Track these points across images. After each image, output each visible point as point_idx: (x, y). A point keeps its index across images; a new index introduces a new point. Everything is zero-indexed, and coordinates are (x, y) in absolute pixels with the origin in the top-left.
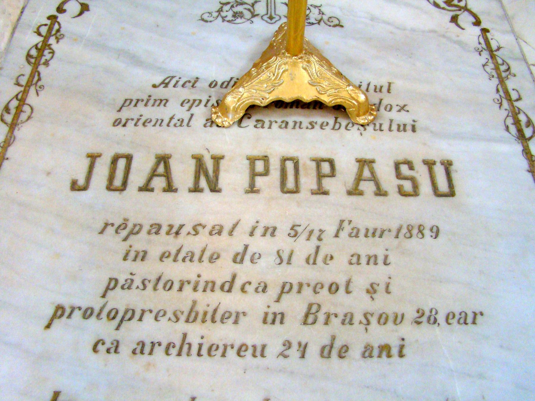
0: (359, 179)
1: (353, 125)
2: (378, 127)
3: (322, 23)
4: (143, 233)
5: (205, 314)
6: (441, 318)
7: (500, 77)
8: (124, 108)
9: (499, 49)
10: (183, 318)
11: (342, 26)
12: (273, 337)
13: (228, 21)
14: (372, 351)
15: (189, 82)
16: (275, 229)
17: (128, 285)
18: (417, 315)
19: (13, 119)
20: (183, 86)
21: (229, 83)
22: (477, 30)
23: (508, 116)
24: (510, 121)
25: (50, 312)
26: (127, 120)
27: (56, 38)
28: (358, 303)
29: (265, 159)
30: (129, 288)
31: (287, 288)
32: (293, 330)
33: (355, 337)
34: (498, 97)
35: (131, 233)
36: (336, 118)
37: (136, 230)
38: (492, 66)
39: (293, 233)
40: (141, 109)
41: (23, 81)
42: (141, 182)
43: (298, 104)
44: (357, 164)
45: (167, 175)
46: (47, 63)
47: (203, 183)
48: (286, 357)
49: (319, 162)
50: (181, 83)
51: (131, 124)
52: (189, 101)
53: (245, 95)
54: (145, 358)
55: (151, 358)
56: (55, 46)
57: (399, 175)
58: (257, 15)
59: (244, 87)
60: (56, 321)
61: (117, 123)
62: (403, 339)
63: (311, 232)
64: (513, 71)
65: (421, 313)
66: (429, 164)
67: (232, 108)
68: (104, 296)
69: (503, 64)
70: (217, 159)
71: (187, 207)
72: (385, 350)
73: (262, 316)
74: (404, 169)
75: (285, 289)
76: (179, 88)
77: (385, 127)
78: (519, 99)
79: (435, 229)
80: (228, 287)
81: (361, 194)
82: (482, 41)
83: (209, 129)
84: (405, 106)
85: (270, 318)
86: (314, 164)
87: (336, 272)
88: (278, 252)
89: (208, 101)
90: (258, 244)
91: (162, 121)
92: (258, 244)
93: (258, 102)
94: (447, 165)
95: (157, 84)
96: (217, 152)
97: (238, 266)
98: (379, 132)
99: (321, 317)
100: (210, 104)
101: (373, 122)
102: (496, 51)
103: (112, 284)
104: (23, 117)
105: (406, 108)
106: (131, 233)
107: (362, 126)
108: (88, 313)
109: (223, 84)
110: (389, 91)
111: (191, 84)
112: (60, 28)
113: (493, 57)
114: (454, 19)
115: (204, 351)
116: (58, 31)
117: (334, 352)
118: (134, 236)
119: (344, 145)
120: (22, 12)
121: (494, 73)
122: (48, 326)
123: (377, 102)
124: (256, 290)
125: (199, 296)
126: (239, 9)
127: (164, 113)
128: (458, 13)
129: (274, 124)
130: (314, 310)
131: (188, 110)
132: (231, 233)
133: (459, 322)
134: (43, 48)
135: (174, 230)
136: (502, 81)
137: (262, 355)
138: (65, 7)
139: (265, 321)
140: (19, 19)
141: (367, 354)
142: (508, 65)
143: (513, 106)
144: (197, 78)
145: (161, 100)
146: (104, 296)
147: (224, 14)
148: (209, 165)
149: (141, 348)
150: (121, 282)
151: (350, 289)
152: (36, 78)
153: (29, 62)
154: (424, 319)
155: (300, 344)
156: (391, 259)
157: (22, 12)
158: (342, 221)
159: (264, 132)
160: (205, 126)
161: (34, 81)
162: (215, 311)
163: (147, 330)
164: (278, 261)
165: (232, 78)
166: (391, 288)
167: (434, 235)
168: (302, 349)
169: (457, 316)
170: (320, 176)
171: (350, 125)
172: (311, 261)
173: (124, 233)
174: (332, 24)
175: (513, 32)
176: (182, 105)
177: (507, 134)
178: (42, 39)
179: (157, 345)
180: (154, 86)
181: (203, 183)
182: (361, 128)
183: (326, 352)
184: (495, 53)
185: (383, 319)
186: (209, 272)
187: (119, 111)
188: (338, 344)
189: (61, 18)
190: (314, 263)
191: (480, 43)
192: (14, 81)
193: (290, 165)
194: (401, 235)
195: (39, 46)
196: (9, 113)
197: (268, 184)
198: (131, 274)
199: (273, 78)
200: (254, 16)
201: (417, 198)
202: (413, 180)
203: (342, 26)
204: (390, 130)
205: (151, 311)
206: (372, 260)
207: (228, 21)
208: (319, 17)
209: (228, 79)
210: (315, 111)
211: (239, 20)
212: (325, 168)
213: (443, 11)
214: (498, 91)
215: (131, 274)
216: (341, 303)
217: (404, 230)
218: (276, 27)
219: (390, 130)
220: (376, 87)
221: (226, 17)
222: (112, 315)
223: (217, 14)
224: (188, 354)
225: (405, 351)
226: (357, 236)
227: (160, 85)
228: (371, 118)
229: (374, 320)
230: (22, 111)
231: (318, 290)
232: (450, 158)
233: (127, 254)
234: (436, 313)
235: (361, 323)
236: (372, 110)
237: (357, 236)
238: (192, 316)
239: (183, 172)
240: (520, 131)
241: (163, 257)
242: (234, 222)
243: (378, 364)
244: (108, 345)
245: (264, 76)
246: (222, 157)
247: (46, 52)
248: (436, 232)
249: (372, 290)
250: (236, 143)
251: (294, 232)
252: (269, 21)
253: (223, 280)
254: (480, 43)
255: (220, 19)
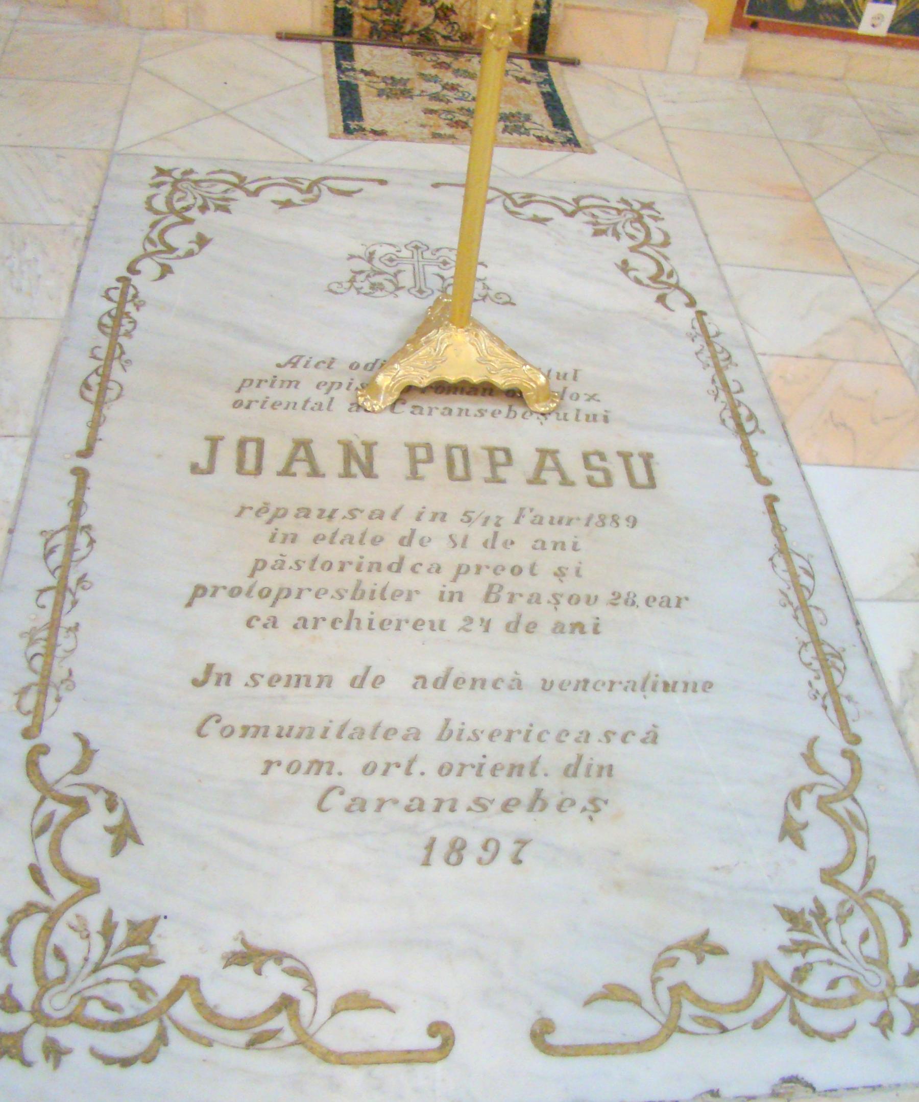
0: (540, 468)
1: (531, 414)
2: (561, 416)
3: (488, 300)
4: (290, 518)
5: (373, 592)
6: (640, 600)
7: (716, 365)
8: (243, 389)
9: (718, 334)
10: (348, 596)
11: (514, 304)
12: (453, 614)
13: (365, 294)
14: (563, 628)
15: (324, 362)
16: (445, 515)
17: (280, 565)
18: (613, 597)
19: (98, 397)
20: (316, 366)
21: (374, 364)
22: (691, 313)
23: (725, 409)
24: (727, 414)
25: (190, 591)
26: (250, 402)
27: (135, 305)
28: (546, 584)
29: (428, 447)
30: (281, 568)
31: (463, 569)
32: (474, 606)
33: (545, 615)
34: (713, 388)
35: (275, 516)
36: (510, 407)
37: (280, 513)
38: (709, 354)
39: (466, 519)
40: (265, 390)
41: (102, 353)
42: (280, 465)
43: (464, 388)
44: (538, 454)
45: (310, 458)
46: (128, 334)
47: (355, 468)
48: (468, 631)
49: (491, 451)
50: (313, 363)
51: (255, 407)
52: (326, 383)
53: (400, 373)
54: (309, 632)
55: (316, 632)
56: (134, 314)
57: (587, 465)
58: (402, 288)
59: (399, 364)
60: (197, 600)
61: (237, 404)
62: (598, 618)
63: (487, 518)
64: (734, 360)
65: (616, 596)
66: (626, 457)
67: (384, 388)
68: (252, 575)
69: (722, 352)
70: (369, 446)
71: (336, 491)
72: (578, 627)
73: (438, 595)
74: (595, 461)
75: (461, 570)
76: (311, 370)
77: (571, 416)
78: (741, 390)
79: (631, 519)
80: (398, 566)
81: (544, 483)
82: (696, 325)
83: (354, 414)
84: (595, 395)
85: (447, 596)
86: (486, 453)
87: (520, 555)
88: (451, 536)
89: (350, 384)
90: (425, 528)
91: (296, 403)
92: (425, 528)
93: (416, 382)
94: (647, 459)
95: (282, 364)
96: (370, 438)
97: (406, 548)
98: (563, 422)
99: (505, 596)
100: (353, 388)
101: (554, 411)
102: (714, 337)
103: (259, 565)
104: (111, 395)
105: (597, 398)
106: (275, 516)
107: (543, 414)
108: (235, 592)
109: (367, 365)
110: (575, 378)
111: (326, 365)
112: (137, 292)
113: (709, 342)
114: (661, 299)
115: (376, 625)
116: (135, 296)
117: (521, 628)
118: (279, 520)
119: (524, 434)
120: (79, 271)
121: (711, 362)
122: (189, 605)
123: (561, 390)
124: (429, 571)
125: (364, 575)
126: (377, 279)
127: (297, 395)
128: (666, 291)
129: (434, 411)
130: (496, 589)
131: (327, 393)
132: (394, 518)
133: (660, 605)
134: (119, 315)
135: (327, 514)
136: (719, 371)
137: (442, 629)
138: (139, 267)
139: (441, 599)
140: (76, 280)
141: (558, 630)
142: (728, 353)
143: (732, 399)
144: (333, 359)
145: (291, 382)
146: (252, 575)
147: (357, 285)
148: (361, 451)
149: (302, 623)
150: (271, 562)
151: (535, 572)
152: (118, 352)
153: (104, 333)
154: (621, 601)
155: (482, 620)
156: (581, 545)
157: (79, 271)
158: (522, 509)
159: (423, 419)
160: (350, 410)
161: (115, 353)
162: (384, 589)
163: (308, 606)
164: (452, 544)
165: (377, 360)
166: (582, 572)
167: (631, 525)
168: (485, 624)
169: (659, 600)
170: (494, 465)
171: (528, 414)
172: (489, 545)
173: (266, 517)
174: (501, 301)
175: (738, 315)
176: (318, 387)
177: (722, 428)
178: (114, 305)
179: (321, 620)
180: (279, 366)
181: (355, 468)
182: (541, 417)
183: (512, 627)
184: (714, 340)
185: (573, 600)
186: (371, 554)
187: (239, 391)
188: (524, 621)
189: (135, 280)
190: (493, 547)
191: (693, 328)
192: (89, 354)
193: (457, 454)
194: (592, 524)
195: (114, 313)
196: (91, 390)
197: (435, 470)
198: (281, 555)
199: (435, 354)
200: (398, 288)
201: (611, 489)
202: (606, 471)
203: (514, 304)
204: (577, 419)
205: (310, 590)
206: (559, 545)
207: (365, 294)
208: (484, 293)
209: (373, 361)
210: (483, 399)
211: (378, 293)
212: (499, 458)
213: (648, 289)
214: (713, 381)
215: (281, 555)
216: (526, 584)
217: (596, 519)
218: (430, 301)
219: (577, 419)
220: (558, 374)
221: (362, 288)
222: (264, 594)
223: (348, 285)
224: (358, 628)
225: (599, 629)
226: (540, 523)
227: (285, 365)
228: (553, 405)
229: (563, 601)
230: (108, 388)
231: (498, 571)
232: (649, 451)
233: (274, 535)
234: (635, 596)
235: (549, 602)
236: (555, 397)
237: (540, 523)
238: (358, 593)
239: (330, 458)
240: (740, 427)
241: (316, 540)
242: (397, 507)
243: (570, 640)
244: (264, 620)
245: (424, 351)
246: (376, 443)
247: (125, 321)
248: (633, 522)
249: (560, 573)
250: (391, 430)
251: (467, 517)
252: (418, 295)
253: (391, 562)
254: (693, 328)
255: (353, 291)
